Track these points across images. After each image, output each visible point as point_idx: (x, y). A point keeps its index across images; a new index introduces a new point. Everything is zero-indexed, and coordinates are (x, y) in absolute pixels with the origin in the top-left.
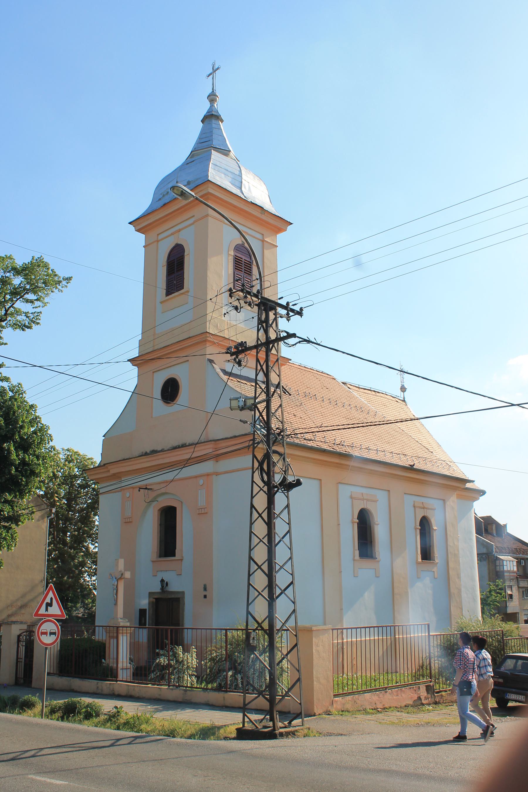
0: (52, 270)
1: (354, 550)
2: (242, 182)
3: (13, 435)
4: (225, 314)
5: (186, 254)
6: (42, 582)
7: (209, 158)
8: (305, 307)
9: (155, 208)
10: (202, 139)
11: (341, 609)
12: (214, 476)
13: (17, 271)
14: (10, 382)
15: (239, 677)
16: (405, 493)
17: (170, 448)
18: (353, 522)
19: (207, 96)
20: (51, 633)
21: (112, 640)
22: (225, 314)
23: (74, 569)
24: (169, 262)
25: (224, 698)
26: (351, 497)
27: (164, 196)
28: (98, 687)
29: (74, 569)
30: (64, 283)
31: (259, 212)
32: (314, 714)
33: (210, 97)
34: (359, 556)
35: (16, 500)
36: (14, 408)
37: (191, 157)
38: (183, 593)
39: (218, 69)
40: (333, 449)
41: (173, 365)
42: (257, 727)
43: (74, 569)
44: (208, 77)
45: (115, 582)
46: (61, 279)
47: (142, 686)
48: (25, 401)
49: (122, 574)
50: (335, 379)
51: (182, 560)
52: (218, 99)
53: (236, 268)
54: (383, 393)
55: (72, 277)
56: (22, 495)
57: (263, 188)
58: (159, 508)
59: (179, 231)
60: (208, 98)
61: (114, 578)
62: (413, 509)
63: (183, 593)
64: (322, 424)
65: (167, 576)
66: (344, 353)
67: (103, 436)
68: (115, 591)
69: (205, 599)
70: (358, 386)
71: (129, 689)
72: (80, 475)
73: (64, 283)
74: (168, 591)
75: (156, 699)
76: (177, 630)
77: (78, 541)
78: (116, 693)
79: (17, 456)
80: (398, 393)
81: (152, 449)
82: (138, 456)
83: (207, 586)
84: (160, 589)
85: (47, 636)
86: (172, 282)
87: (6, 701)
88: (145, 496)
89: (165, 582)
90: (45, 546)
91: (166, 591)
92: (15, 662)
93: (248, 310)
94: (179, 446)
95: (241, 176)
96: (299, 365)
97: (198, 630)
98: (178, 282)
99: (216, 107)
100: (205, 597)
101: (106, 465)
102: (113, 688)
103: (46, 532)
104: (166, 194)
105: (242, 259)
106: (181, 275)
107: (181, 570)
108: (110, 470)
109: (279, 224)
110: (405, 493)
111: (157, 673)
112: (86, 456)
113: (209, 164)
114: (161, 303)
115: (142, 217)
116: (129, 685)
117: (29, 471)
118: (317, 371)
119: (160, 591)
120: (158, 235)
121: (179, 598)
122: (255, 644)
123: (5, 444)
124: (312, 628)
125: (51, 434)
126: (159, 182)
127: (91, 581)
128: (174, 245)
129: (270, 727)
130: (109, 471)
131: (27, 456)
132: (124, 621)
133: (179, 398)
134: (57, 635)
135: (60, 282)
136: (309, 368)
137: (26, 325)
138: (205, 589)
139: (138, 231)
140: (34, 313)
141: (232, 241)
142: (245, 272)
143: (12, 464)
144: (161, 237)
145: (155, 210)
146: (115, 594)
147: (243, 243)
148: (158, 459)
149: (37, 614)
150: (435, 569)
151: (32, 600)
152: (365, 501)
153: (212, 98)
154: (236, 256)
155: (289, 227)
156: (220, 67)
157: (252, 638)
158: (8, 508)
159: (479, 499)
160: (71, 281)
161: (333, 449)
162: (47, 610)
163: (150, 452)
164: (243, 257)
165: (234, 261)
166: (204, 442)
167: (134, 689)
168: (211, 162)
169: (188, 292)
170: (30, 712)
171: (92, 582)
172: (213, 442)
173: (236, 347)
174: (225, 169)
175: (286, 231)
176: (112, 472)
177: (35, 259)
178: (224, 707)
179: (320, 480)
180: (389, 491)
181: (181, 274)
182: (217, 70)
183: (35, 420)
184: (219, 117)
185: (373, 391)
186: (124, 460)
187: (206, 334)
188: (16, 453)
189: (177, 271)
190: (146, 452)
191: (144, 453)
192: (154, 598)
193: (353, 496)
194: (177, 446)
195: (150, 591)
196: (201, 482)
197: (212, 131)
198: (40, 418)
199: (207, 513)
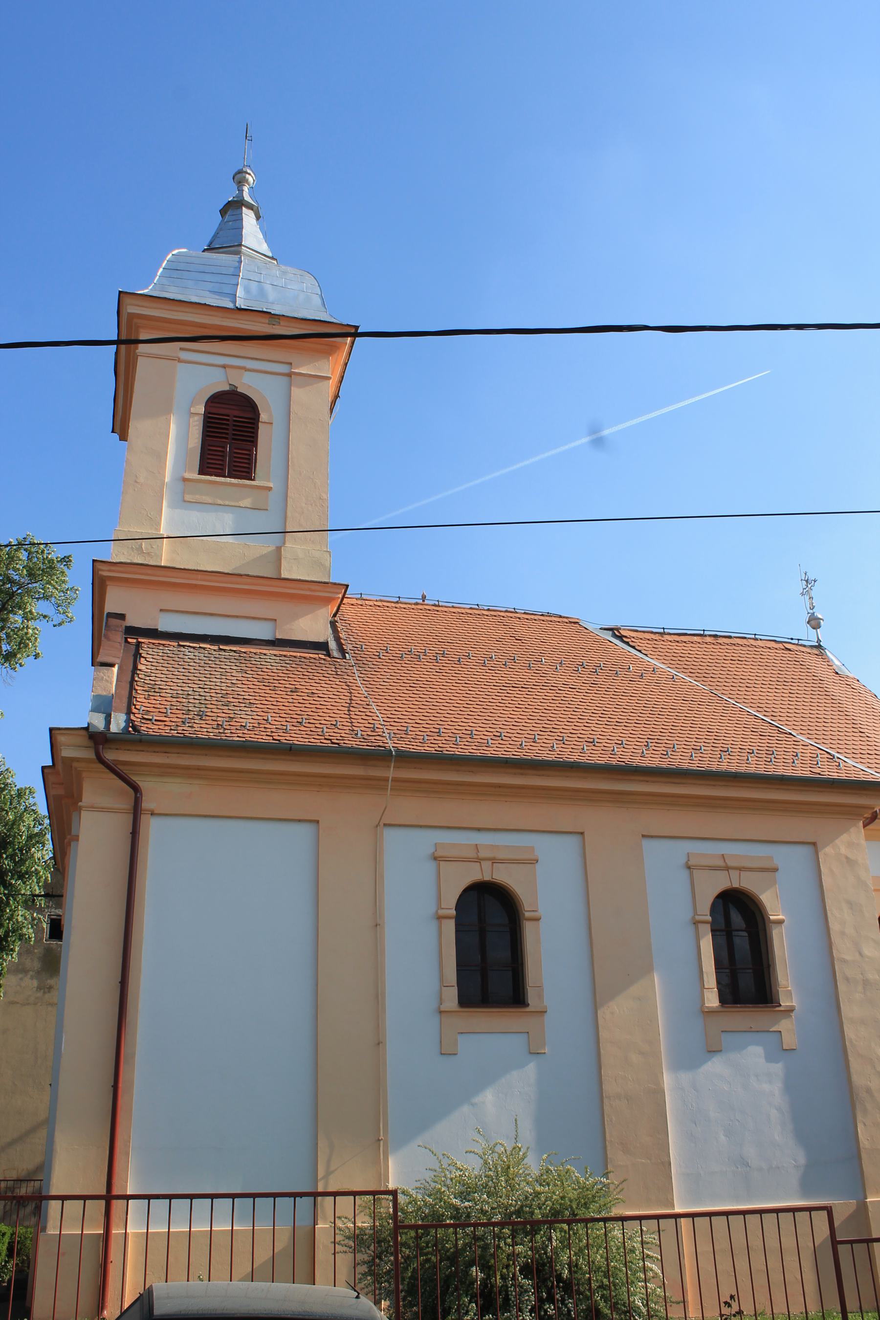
16: (643, 836)
19: (234, 173)
60: (233, 179)
80: (809, 636)
105: (228, 416)
110: (643, 836)
142: (234, 439)
150: (785, 1025)
180: (582, 833)
185: (710, 636)
195: (833, 1208)
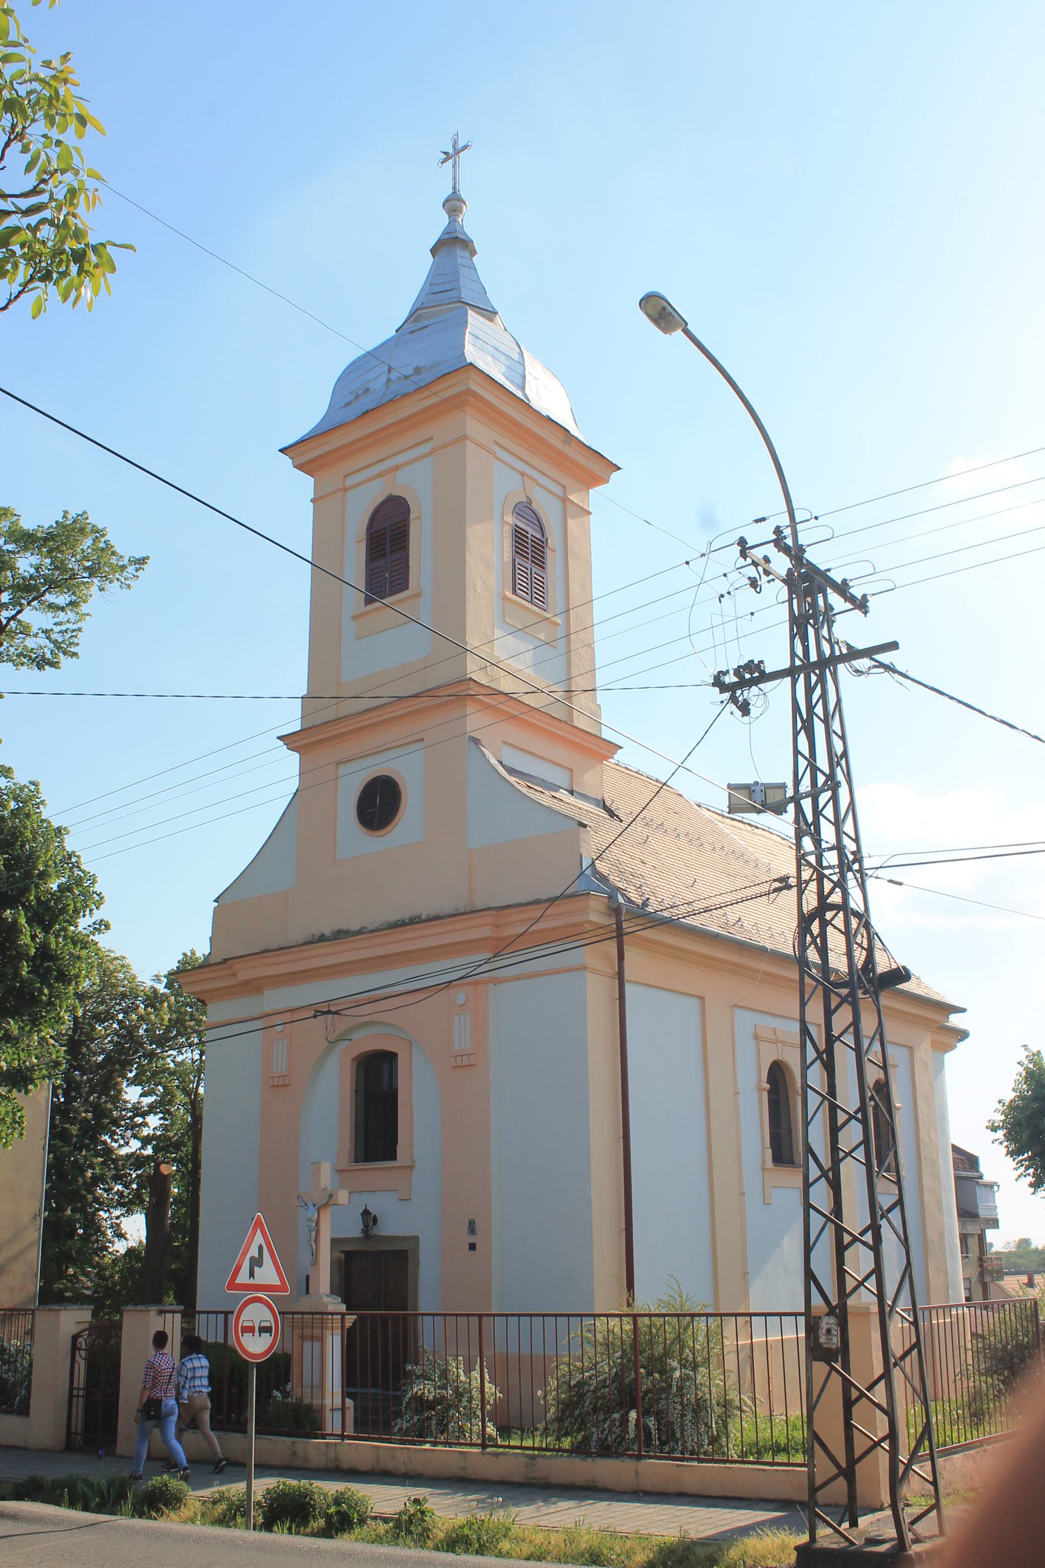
0: (105, 542)
1: (763, 1149)
2: (524, 377)
3: (26, 890)
4: (722, 596)
5: (412, 516)
6: (37, 1219)
7: (465, 323)
8: (873, 595)
9: (338, 419)
10: (436, 285)
11: (746, 1274)
12: (491, 985)
13: (27, 540)
14: (13, 779)
15: (651, 1422)
17: (381, 925)
18: (760, 1090)
20: (263, 1330)
21: (307, 1345)
22: (722, 596)
23: (84, 1192)
24: (371, 534)
25: (636, 1471)
26: (756, 1037)
27: (357, 396)
28: (294, 1453)
29: (85, 1193)
30: (131, 569)
31: (560, 439)
32: (881, 1506)
33: (449, 203)
34: (773, 1162)
35: (43, 1034)
36: (24, 834)
37: (415, 321)
38: (415, 1239)
39: (465, 147)
40: (729, 933)
41: (386, 750)
42: (852, 1543)
43: (85, 1193)
44: (442, 163)
45: (313, 1214)
46: (126, 562)
47: (415, 1449)
48: (42, 821)
49: (331, 1196)
50: (681, 795)
51: (411, 1167)
52: (464, 207)
53: (516, 552)
54: (764, 830)
55: (148, 557)
56: (35, 1022)
57: (561, 393)
58: (355, 1054)
59: (396, 468)
60: (443, 207)
61: (310, 1204)
62: (752, 1044)
63: (415, 1239)
64: (695, 881)
65: (377, 1204)
66: (951, 698)
67: (214, 901)
68: (314, 1234)
69: (472, 1252)
70: (720, 812)
71: (378, 1456)
72: (100, 991)
73: (131, 569)
74: (379, 1236)
75: (453, 1477)
76: (405, 1318)
77: (91, 1132)
78: (345, 1466)
79: (33, 937)
81: (337, 928)
82: (301, 942)
83: (477, 1224)
84: (360, 1231)
85: (253, 1335)
86: (380, 574)
87: (105, 1491)
88: (326, 1028)
89: (372, 1216)
90: (43, 1141)
91: (374, 1235)
92: (67, 1395)
93: (540, 639)
94: (403, 921)
95: (522, 363)
96: (616, 764)
97: (458, 1317)
98: (393, 574)
99: (460, 221)
100: (472, 1247)
101: (229, 962)
102: (336, 1455)
103: (45, 1111)
104: (363, 393)
105: (527, 533)
106: (401, 561)
107: (411, 1189)
108: (238, 973)
109: (596, 468)
111: (412, 1418)
112: (112, 952)
113: (465, 334)
114: (354, 618)
115: (312, 437)
116: (378, 1447)
117: (55, 973)
118: (648, 777)
119: (361, 1235)
120: (345, 476)
121: (405, 1252)
122: (833, 1344)
123: (8, 911)
124: (869, 1308)
125: (101, 893)
126: (343, 370)
127: (112, 1219)
128: (385, 498)
129: (891, 1540)
130: (235, 975)
131: (52, 939)
132: (335, 1301)
133: (399, 820)
134: (273, 1334)
135: (123, 568)
136: (634, 770)
137: (47, 657)
138: (472, 1228)
139: (299, 467)
140: (66, 631)
141: (507, 496)
143: (21, 955)
144: (351, 481)
145: (344, 424)
146: (313, 1239)
147: (529, 501)
148: (358, 949)
149: (233, 1285)
151: (15, 1258)
152: (780, 1045)
153: (453, 205)
154: (516, 526)
155: (615, 476)
156: (470, 143)
157: (824, 1331)
158: (11, 1053)
159: (956, 1047)
160: (145, 567)
161: (729, 933)
162: (252, 1274)
163: (332, 933)
164: (531, 531)
165: (514, 536)
166: (465, 913)
167: (393, 1456)
168: (468, 330)
169: (418, 595)
170: (172, 1515)
171: (113, 1221)
172: (493, 912)
173: (737, 672)
174: (493, 347)
175: (608, 482)
176: (242, 976)
177: (69, 516)
178: (641, 1495)
179: (702, 998)
181: (402, 558)
182: (463, 150)
183: (69, 860)
184: (469, 244)
186: (281, 949)
187: (469, 684)
188: (30, 931)
189: (391, 552)
190: (322, 933)
191: (316, 937)
192: (341, 1251)
193: (760, 1034)
194: (398, 921)
196: (461, 997)
197: (458, 272)
198: (78, 857)
199: (474, 1065)
